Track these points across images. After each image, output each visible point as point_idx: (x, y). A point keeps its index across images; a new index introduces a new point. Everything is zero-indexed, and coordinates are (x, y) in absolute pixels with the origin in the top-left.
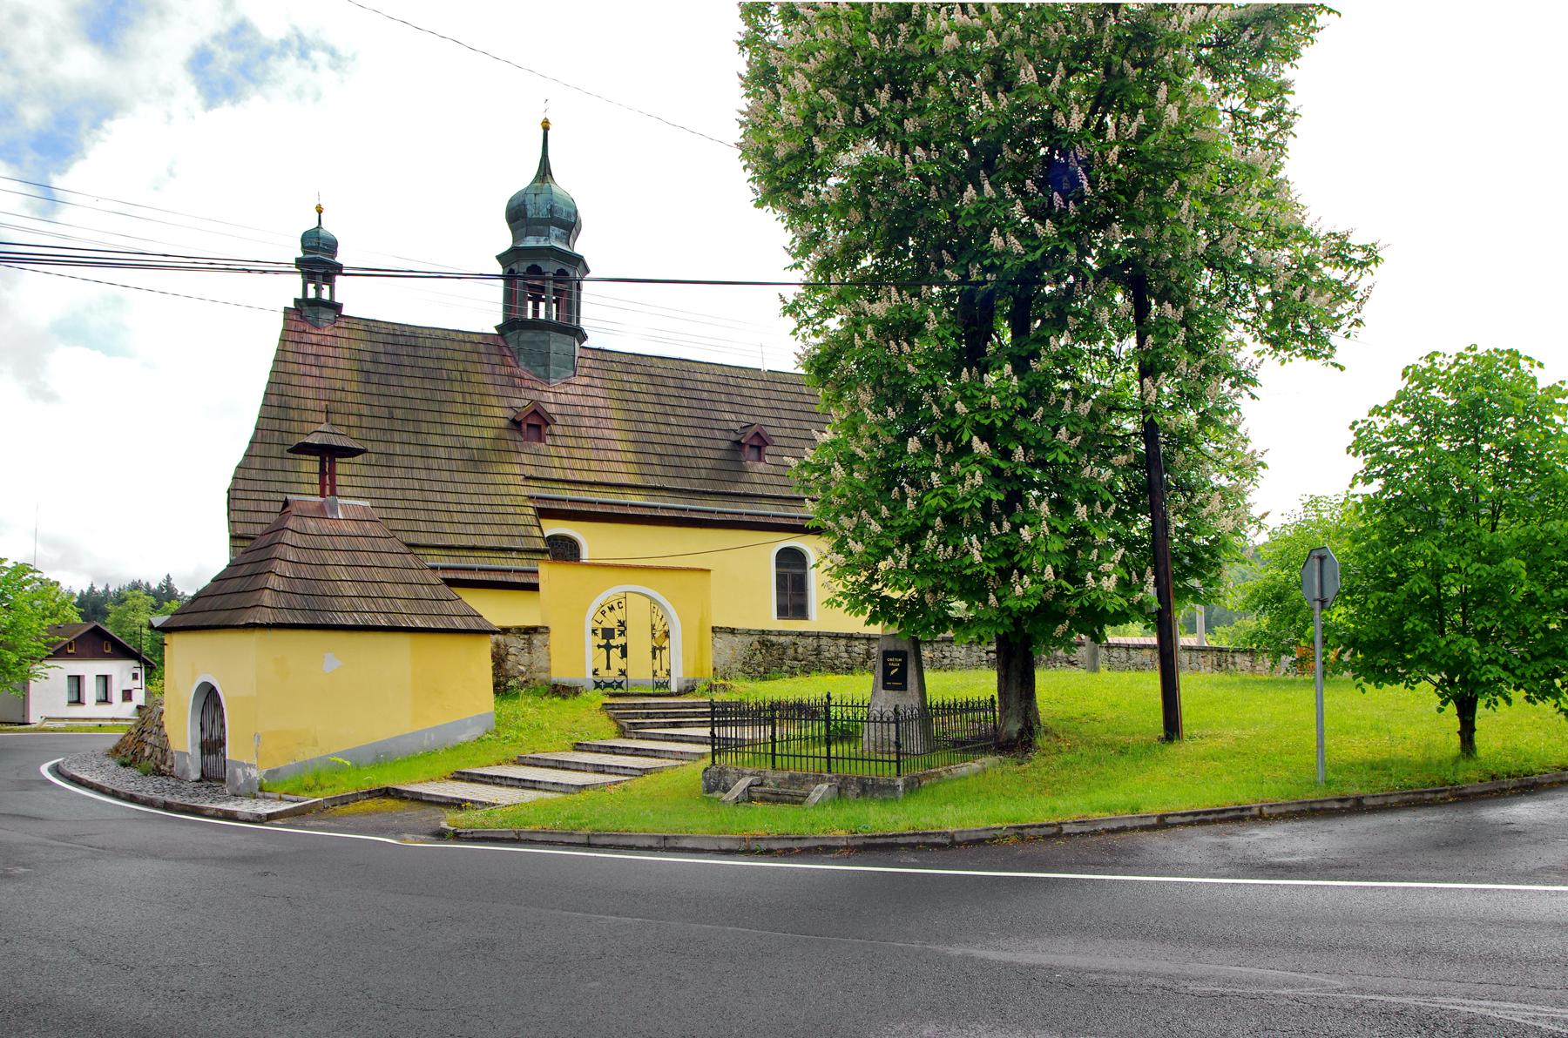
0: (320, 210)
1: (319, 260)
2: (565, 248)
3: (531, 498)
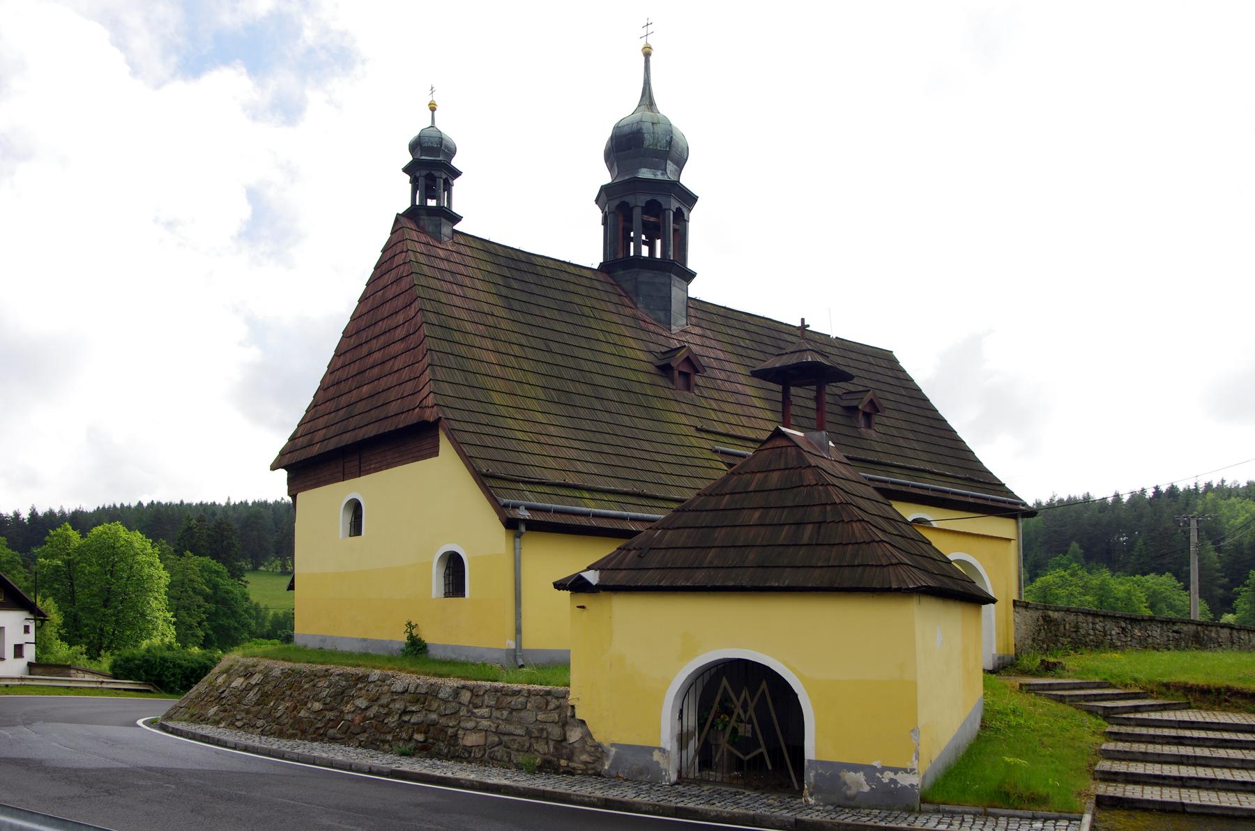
1: (431, 165)
3: (716, 452)
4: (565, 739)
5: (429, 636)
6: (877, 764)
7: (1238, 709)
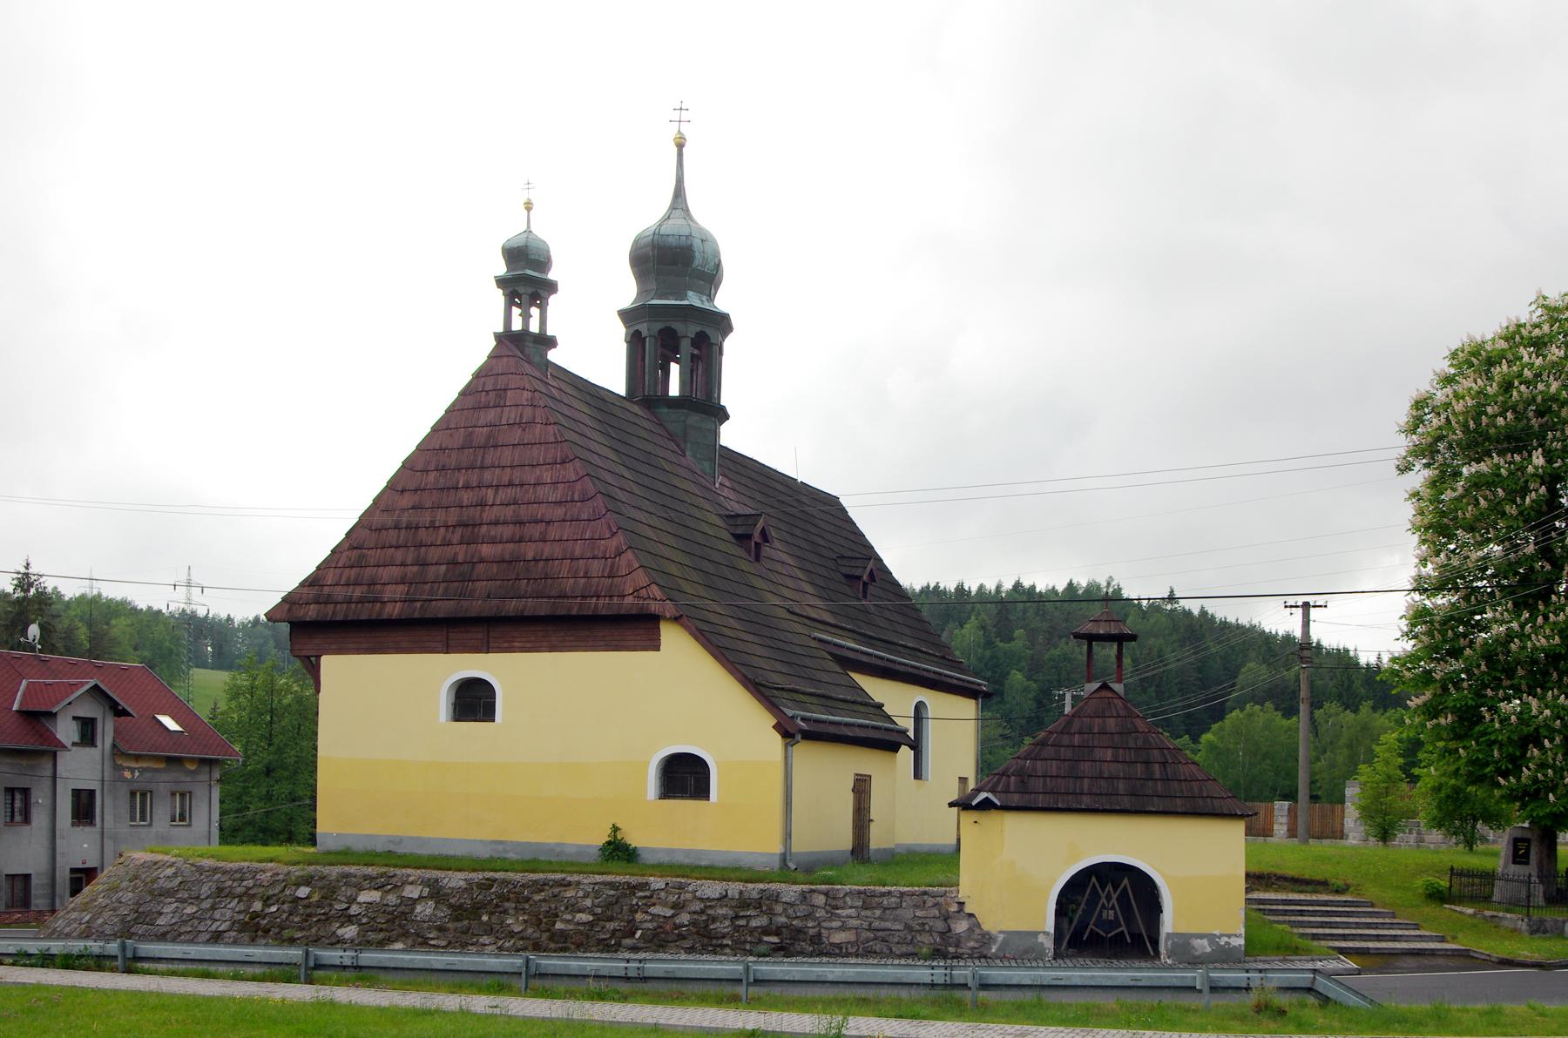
0: (529, 206)
2: (706, 306)
5: (635, 839)
6: (1217, 932)
7: (1285, 890)
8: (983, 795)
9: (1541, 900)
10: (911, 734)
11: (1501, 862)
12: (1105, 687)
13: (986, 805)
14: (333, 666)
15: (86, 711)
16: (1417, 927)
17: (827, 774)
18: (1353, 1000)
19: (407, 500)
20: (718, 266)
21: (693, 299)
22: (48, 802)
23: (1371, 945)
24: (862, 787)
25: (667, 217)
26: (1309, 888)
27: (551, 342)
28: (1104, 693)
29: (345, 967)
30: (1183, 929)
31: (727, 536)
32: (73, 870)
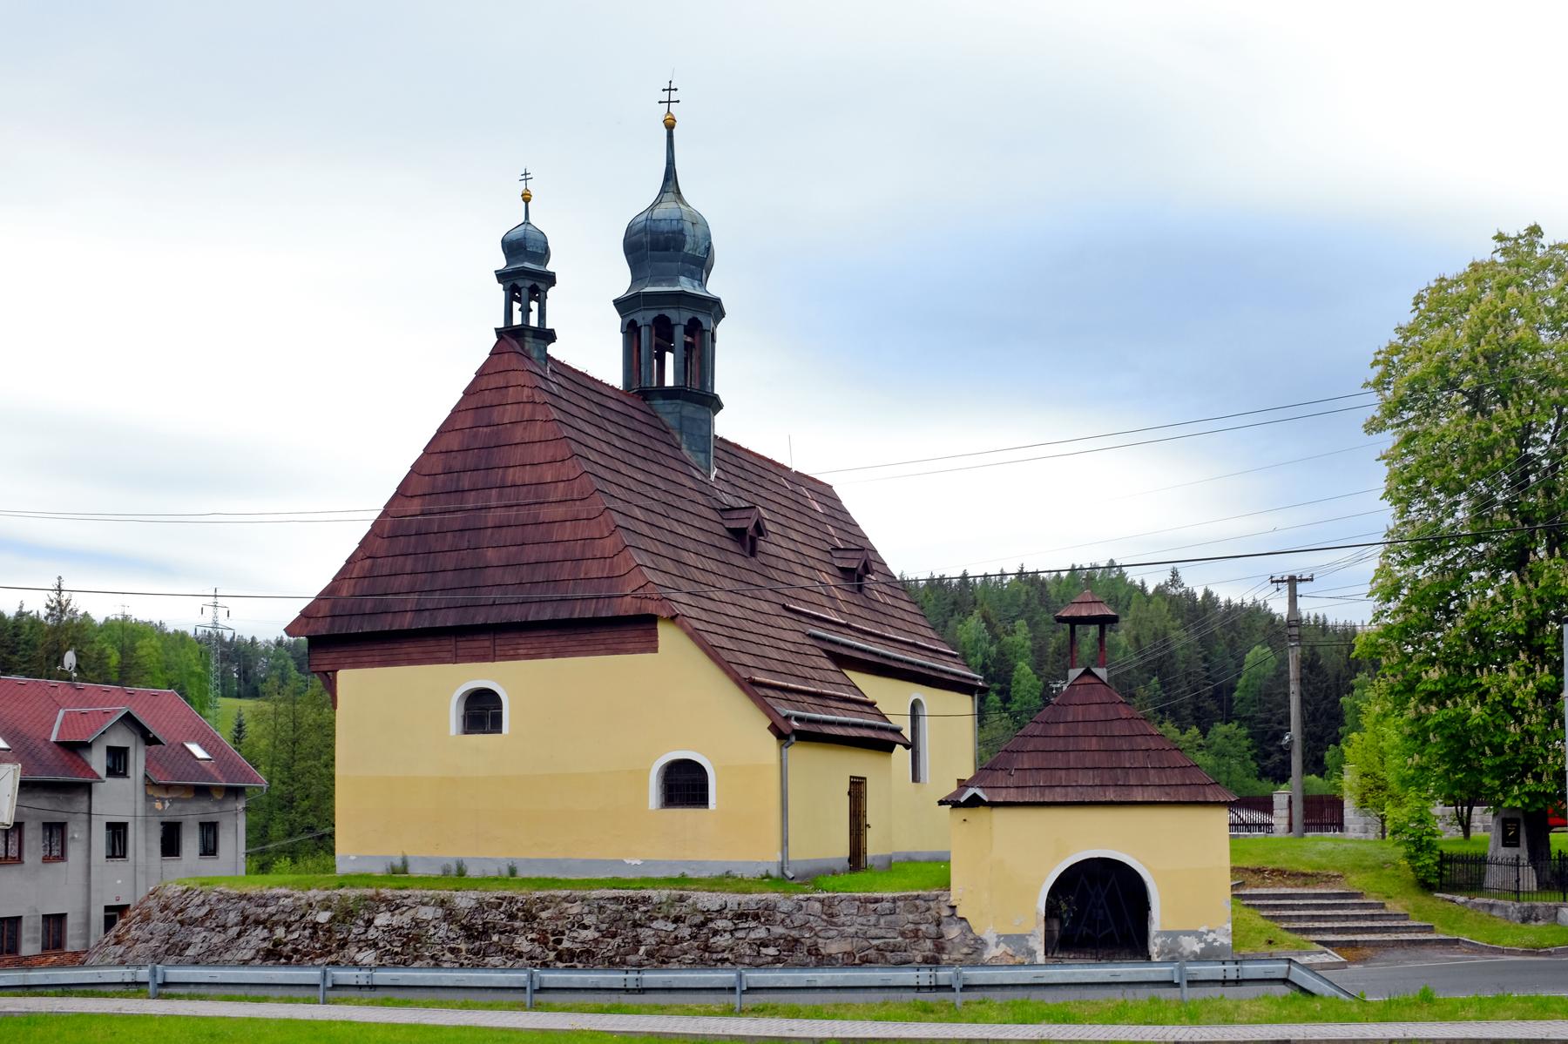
0: (526, 198)
4: (942, 936)
6: (1203, 929)
8: (970, 792)
9: (1533, 885)
10: (907, 733)
11: (1491, 845)
12: (1088, 672)
13: (974, 802)
14: (347, 679)
15: (117, 740)
16: (1430, 929)
17: (824, 774)
18: (1327, 990)
19: (415, 506)
20: (709, 249)
21: (685, 285)
22: (84, 836)
23: (1359, 937)
24: (857, 788)
25: (659, 201)
26: (1299, 882)
27: (550, 336)
28: (1087, 679)
29: (360, 987)
30: (1171, 927)
31: (723, 532)
32: (107, 908)
